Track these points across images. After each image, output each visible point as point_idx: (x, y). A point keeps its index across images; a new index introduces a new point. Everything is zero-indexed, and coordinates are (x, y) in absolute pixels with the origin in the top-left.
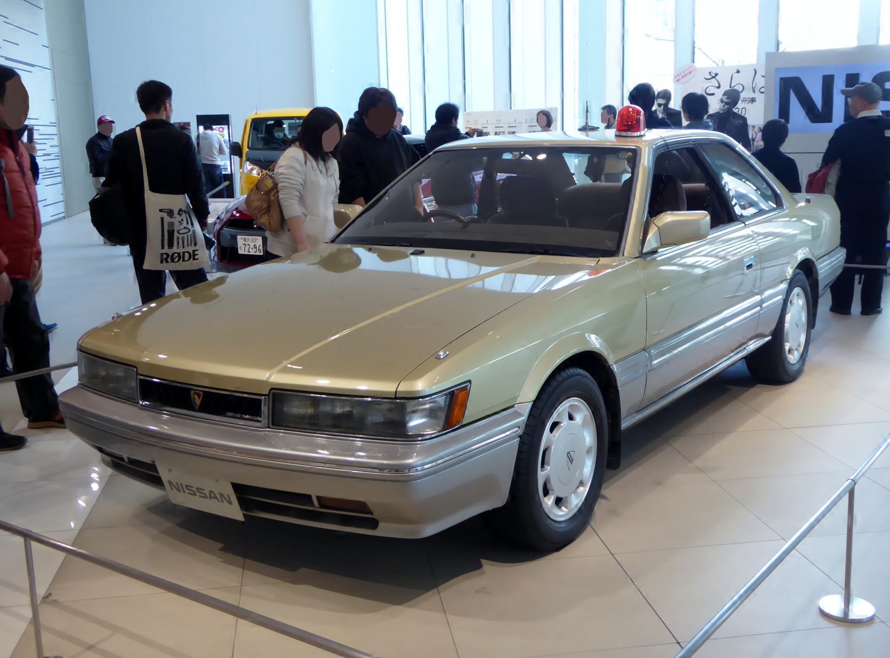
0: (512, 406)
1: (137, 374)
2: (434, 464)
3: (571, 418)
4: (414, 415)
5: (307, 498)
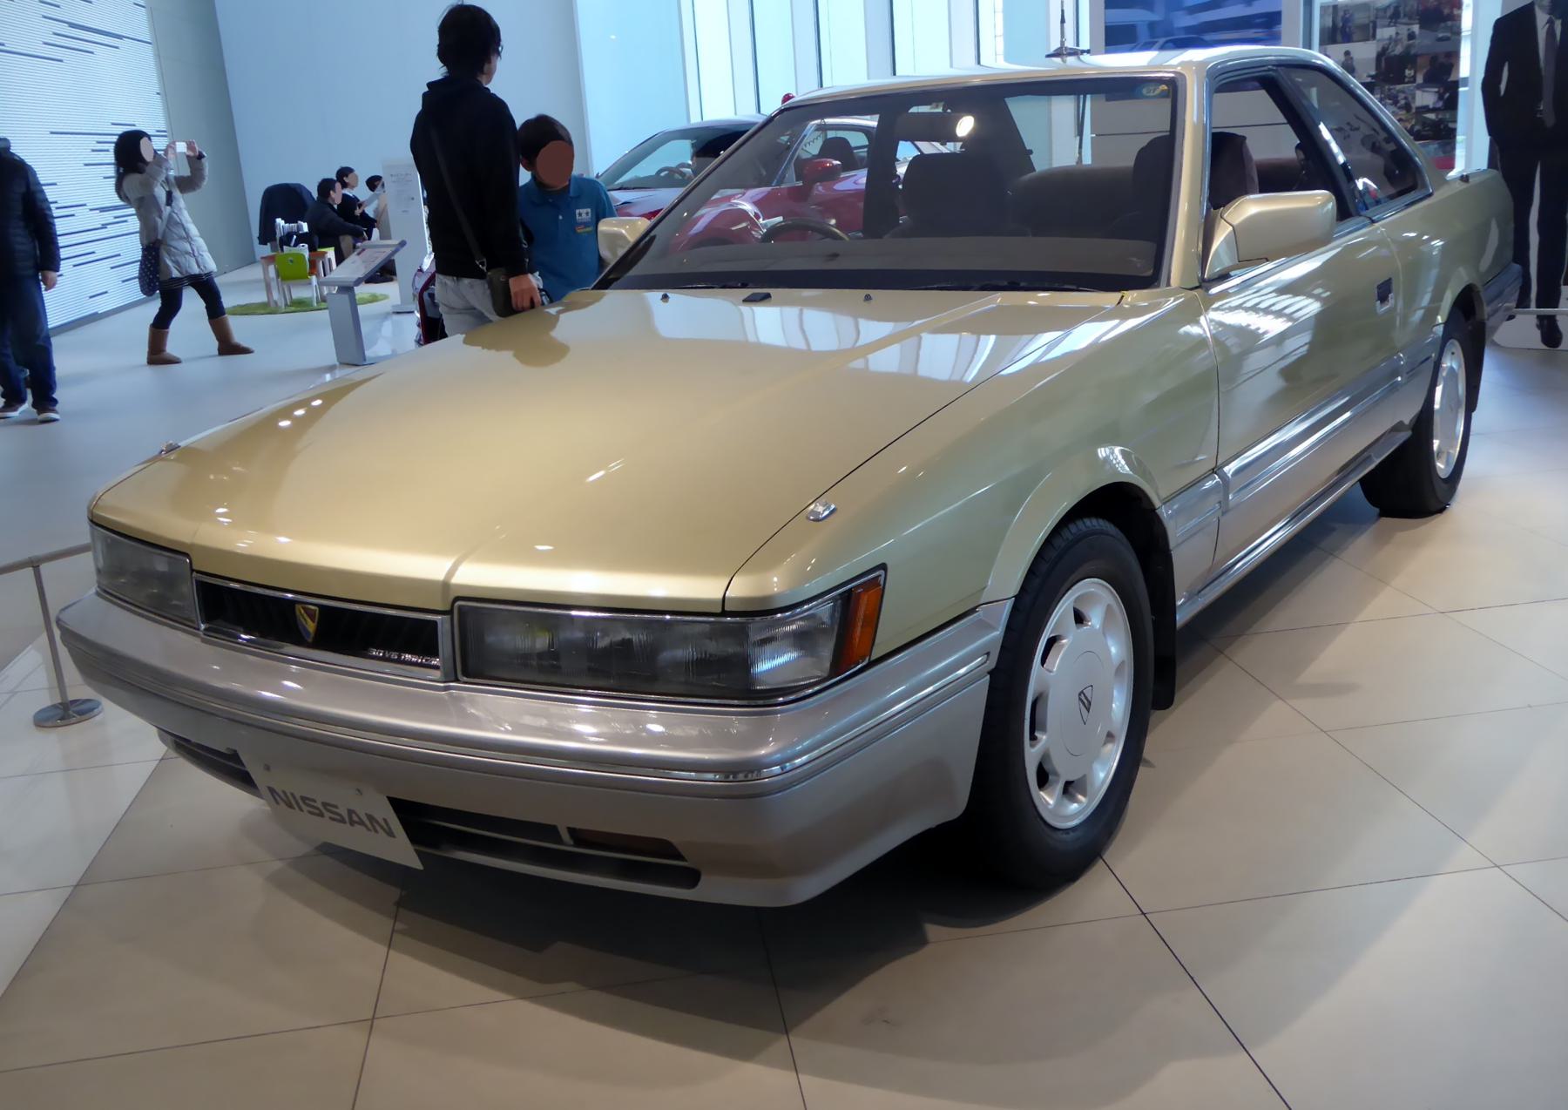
0: (973, 610)
1: (193, 570)
2: (815, 753)
3: (1080, 618)
4: (768, 648)
5: (550, 832)
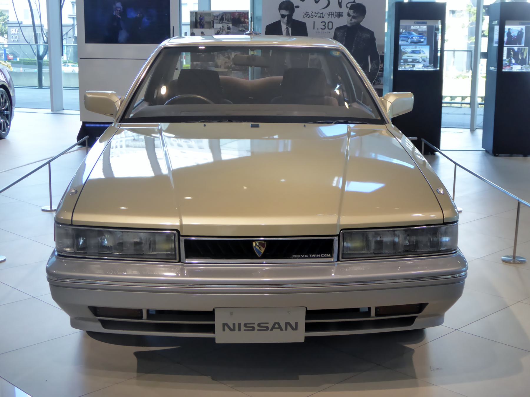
5: (137, 313)
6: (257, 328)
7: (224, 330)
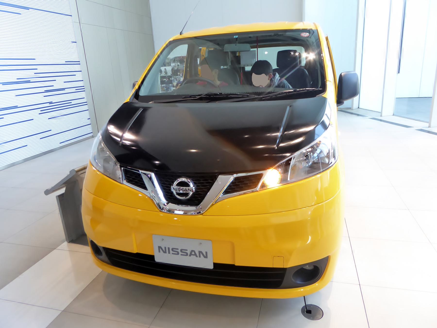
6: (180, 253)
7: (206, 253)
